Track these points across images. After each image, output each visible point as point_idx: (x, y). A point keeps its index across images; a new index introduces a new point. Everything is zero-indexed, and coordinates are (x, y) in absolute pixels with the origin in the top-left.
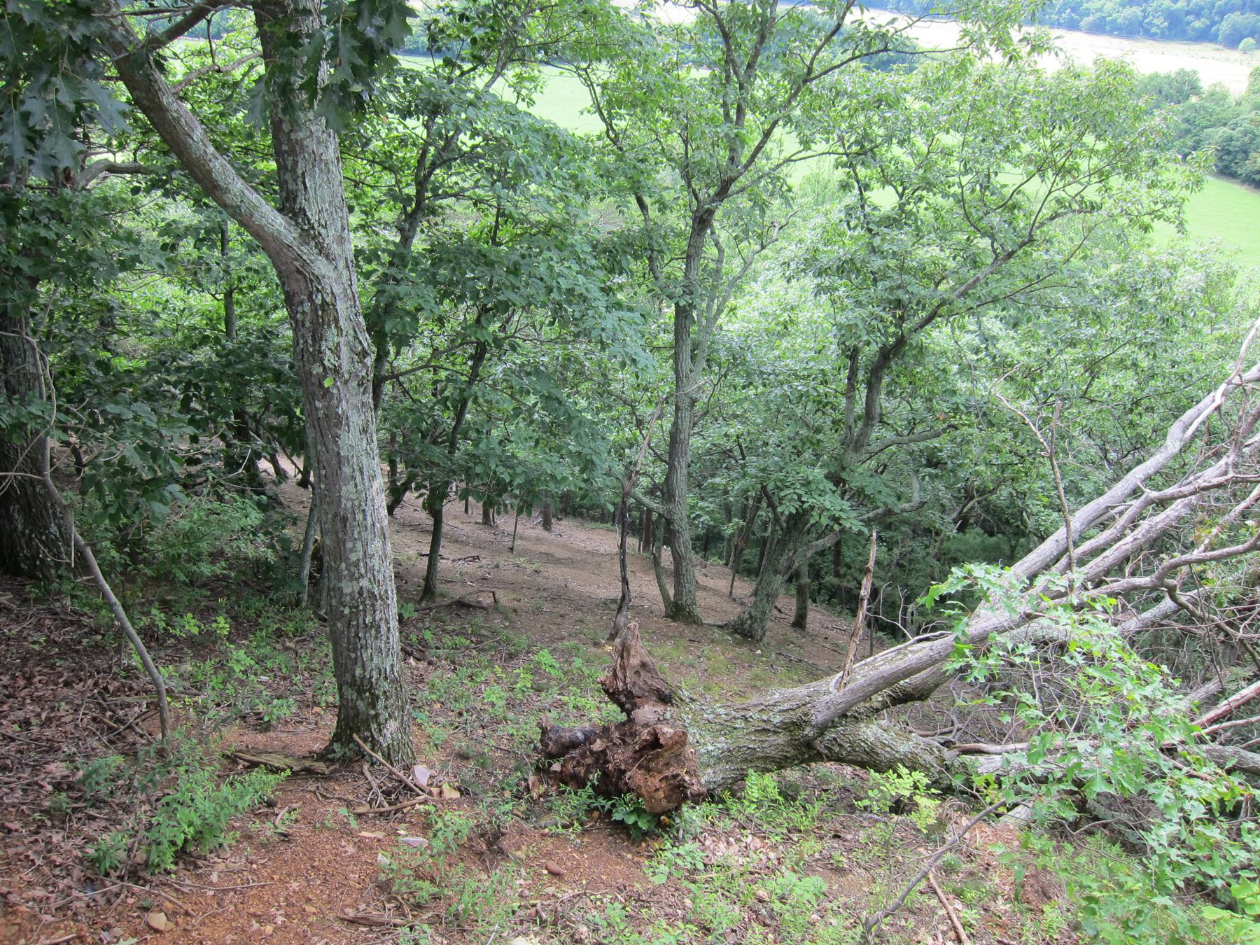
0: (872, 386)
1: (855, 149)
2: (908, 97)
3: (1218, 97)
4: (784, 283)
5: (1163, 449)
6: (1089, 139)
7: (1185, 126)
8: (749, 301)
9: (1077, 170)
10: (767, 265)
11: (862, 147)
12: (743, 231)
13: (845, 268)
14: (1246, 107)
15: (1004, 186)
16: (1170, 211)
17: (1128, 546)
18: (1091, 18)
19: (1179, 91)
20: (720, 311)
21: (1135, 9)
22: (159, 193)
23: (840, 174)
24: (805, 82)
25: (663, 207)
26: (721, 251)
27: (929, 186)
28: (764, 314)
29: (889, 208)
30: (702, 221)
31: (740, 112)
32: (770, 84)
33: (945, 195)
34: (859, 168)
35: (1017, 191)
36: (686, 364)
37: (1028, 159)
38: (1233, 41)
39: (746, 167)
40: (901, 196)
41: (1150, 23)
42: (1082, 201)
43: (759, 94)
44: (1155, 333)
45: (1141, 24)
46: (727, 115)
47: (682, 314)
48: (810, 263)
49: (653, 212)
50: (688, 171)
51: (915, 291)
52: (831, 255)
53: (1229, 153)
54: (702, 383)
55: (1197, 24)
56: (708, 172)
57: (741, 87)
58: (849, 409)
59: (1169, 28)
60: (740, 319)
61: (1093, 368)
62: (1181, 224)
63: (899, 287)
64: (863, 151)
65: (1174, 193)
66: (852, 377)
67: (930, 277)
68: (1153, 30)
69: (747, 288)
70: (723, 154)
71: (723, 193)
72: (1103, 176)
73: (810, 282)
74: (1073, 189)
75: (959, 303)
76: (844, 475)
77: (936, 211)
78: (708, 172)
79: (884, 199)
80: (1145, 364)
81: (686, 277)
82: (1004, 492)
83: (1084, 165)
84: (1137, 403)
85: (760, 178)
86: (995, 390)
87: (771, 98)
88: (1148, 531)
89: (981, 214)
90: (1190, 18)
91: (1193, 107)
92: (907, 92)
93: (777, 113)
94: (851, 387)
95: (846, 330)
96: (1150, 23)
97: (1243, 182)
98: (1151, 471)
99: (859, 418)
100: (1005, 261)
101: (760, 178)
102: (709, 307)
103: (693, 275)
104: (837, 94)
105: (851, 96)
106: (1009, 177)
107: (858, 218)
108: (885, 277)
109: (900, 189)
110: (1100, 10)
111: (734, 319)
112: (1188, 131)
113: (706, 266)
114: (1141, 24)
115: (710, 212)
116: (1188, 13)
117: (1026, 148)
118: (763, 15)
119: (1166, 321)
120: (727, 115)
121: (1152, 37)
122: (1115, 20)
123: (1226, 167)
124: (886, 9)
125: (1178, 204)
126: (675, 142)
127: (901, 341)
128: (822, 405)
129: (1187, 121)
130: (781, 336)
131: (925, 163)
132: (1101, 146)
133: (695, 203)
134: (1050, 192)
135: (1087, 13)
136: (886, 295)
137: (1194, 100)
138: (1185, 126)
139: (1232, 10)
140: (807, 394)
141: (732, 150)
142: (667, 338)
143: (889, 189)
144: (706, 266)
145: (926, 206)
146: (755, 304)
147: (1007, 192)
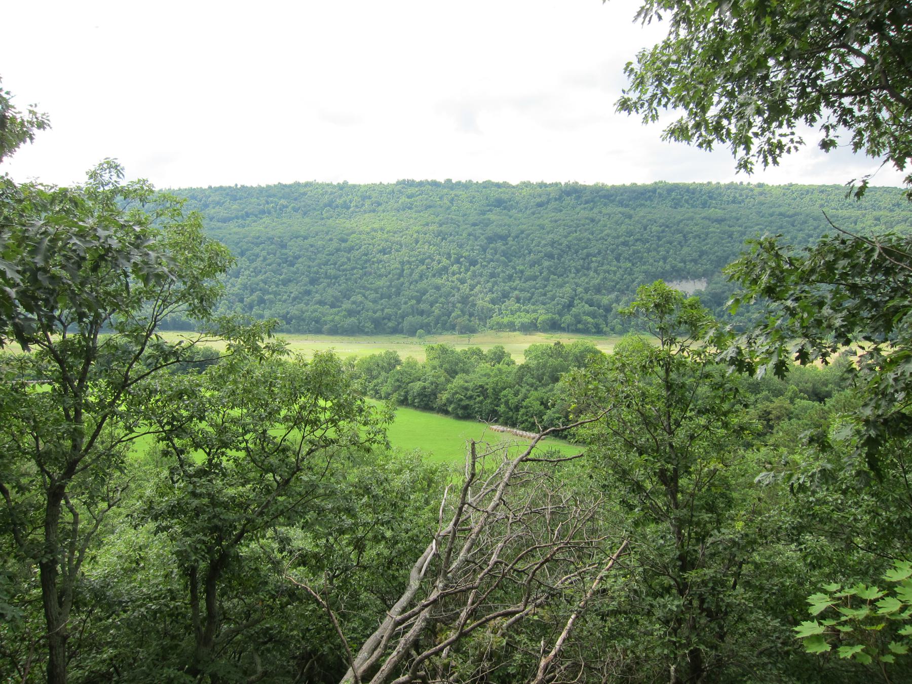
0: (210, 592)
1: (167, 428)
2: (203, 390)
3: (412, 365)
4: (133, 531)
5: (409, 588)
6: (321, 402)
7: (398, 384)
8: (108, 550)
9: (320, 421)
10: (118, 517)
11: (173, 426)
12: (89, 498)
13: (174, 511)
14: (428, 369)
15: (275, 438)
16: (379, 437)
17: (395, 658)
18: (328, 326)
19: (389, 364)
20: (80, 561)
21: (353, 319)
22: (185, 306)
23: (162, 445)
24: (123, 387)
25: (21, 489)
26: (76, 515)
27: (225, 445)
28: (120, 557)
29: (200, 464)
30: (55, 494)
31: (78, 414)
32: (100, 391)
33: (238, 449)
34: (176, 440)
35: (284, 440)
36: (55, 608)
37: (286, 419)
38: (412, 332)
39: (86, 451)
40: (209, 454)
41: (363, 326)
42: (326, 440)
43: (92, 399)
44: (388, 515)
45: (358, 327)
46: (67, 416)
47: (48, 571)
48: (150, 512)
49: (13, 494)
50: (41, 458)
51: (226, 517)
52: (163, 503)
53: (426, 396)
54: (72, 621)
55: (390, 324)
56: (56, 459)
57: (76, 395)
58: (195, 615)
59: (375, 328)
60: (99, 566)
61: (359, 545)
62: (387, 444)
63: (215, 517)
64: (175, 428)
65: (379, 426)
66: (193, 591)
67: (240, 505)
68: (366, 330)
69: (105, 541)
70: (68, 443)
71: (70, 471)
72: (333, 421)
73: (151, 525)
74: (319, 433)
75: (259, 521)
76: (200, 667)
77: (235, 460)
78: (56, 459)
79: (199, 457)
80: (389, 534)
81: (47, 540)
82: (326, 649)
83: (322, 417)
84: (391, 562)
85: (99, 456)
86: (295, 575)
87: (101, 400)
88: (405, 644)
89: (263, 458)
90: (386, 321)
91: (398, 372)
92: (201, 386)
93: (106, 410)
94: (195, 599)
95: (181, 555)
96: (363, 326)
97: (438, 412)
98: (405, 604)
99: (205, 619)
100: (285, 486)
101: (99, 456)
102: (70, 560)
103: (53, 538)
104: (151, 392)
105: (162, 392)
106: (277, 432)
107: (179, 474)
108: (204, 512)
109: (208, 450)
110: (332, 321)
111: (96, 567)
112: (400, 386)
113: (64, 528)
114: (358, 327)
115: (62, 487)
116: (384, 319)
117: (283, 412)
118: (88, 346)
119: (394, 505)
120: (67, 416)
121: (367, 334)
122: (342, 326)
123: (427, 405)
124: (194, 331)
125: (383, 432)
126: (28, 441)
127: (224, 556)
128: (175, 615)
129: (398, 380)
130: (135, 571)
131: (221, 430)
132: (329, 404)
133: (48, 480)
134: (304, 437)
135: (325, 323)
136: (206, 524)
137: (398, 368)
138: (398, 384)
139: (407, 315)
140: (159, 611)
141: (74, 440)
142: (37, 592)
143: (200, 451)
144: (64, 528)
145: (229, 458)
146: (113, 551)
147: (279, 440)
